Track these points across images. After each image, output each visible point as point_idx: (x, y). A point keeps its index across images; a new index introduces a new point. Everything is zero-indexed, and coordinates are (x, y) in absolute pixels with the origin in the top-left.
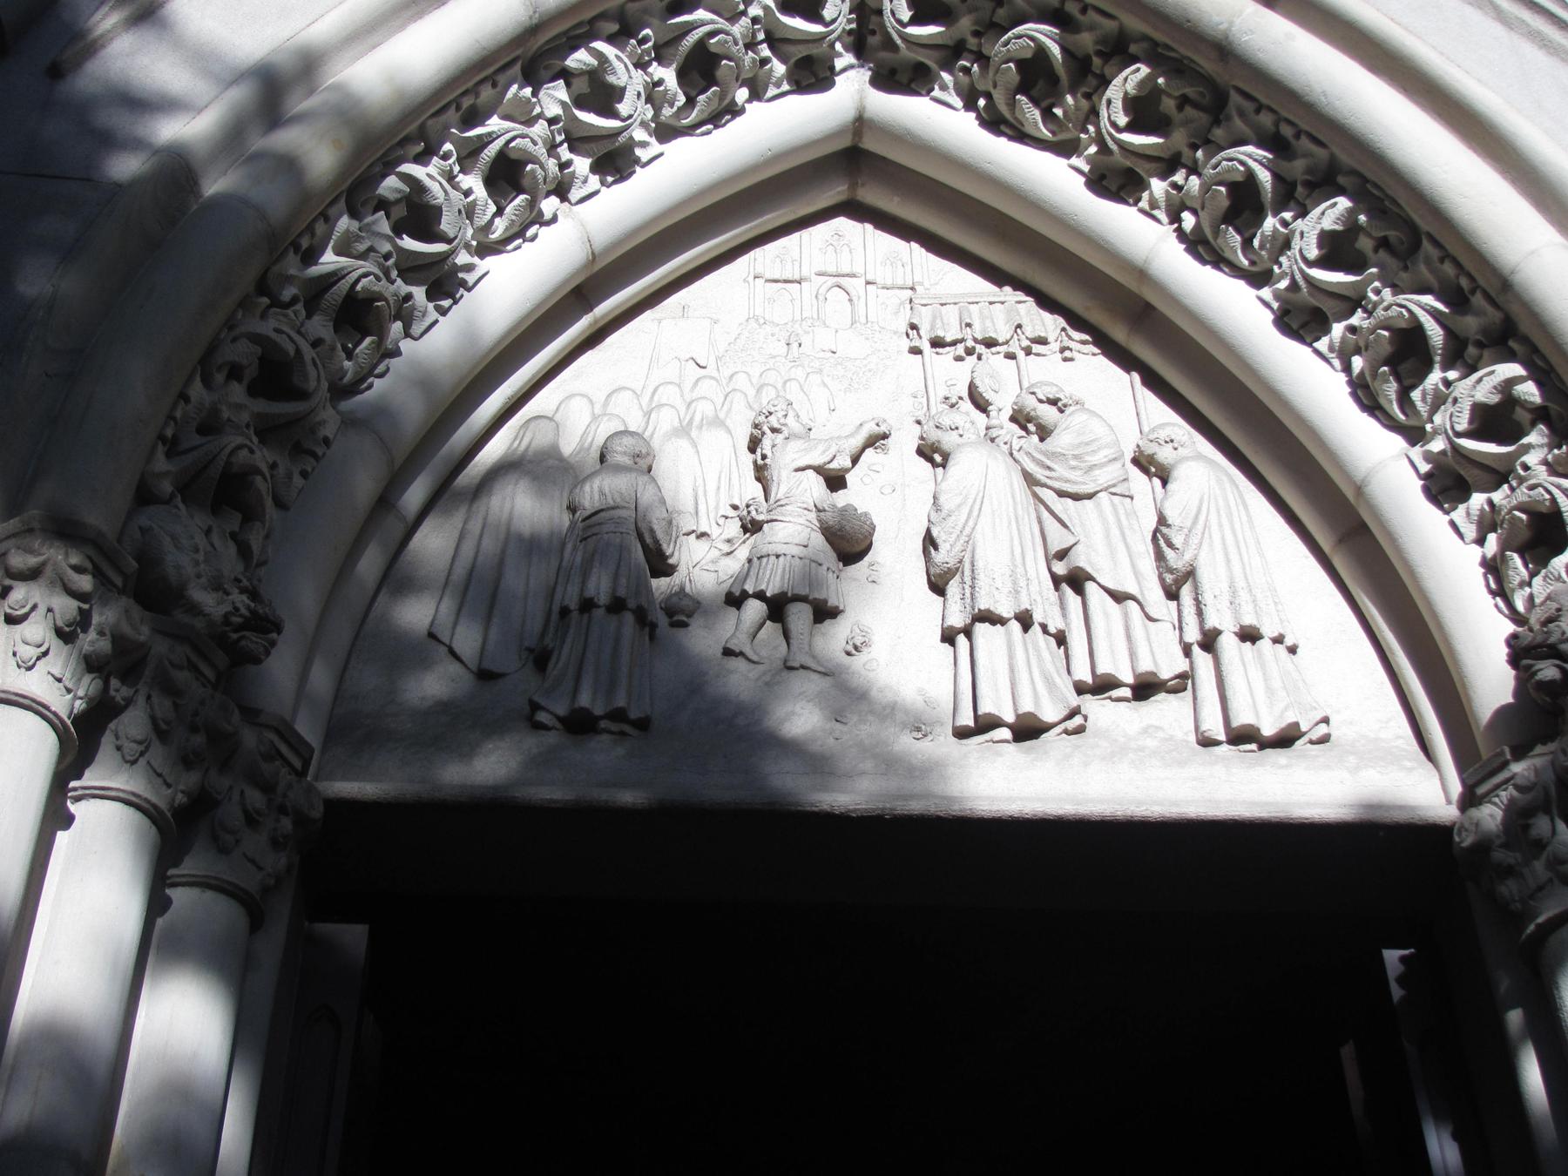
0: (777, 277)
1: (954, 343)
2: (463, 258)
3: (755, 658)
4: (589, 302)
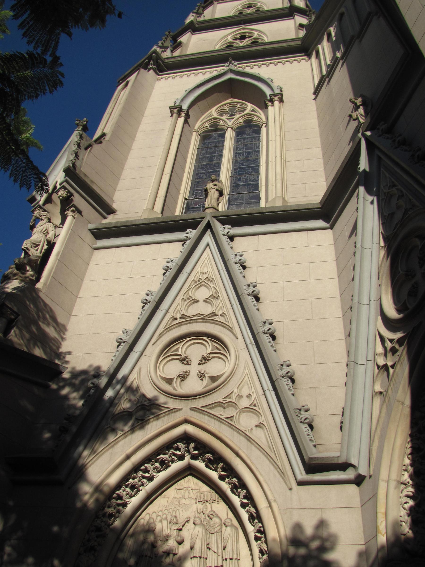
4: (150, 498)
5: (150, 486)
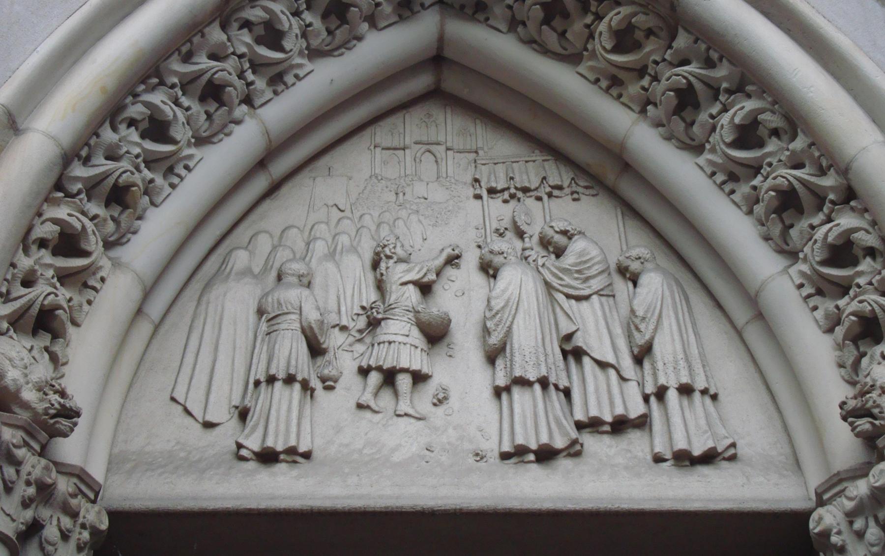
0: (389, 145)
1: (503, 190)
2: (187, 152)
3: (377, 409)
5: (281, 110)
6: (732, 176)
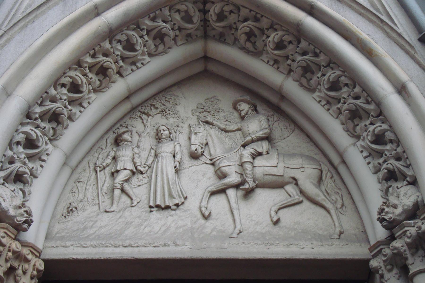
6: (329, 103)
